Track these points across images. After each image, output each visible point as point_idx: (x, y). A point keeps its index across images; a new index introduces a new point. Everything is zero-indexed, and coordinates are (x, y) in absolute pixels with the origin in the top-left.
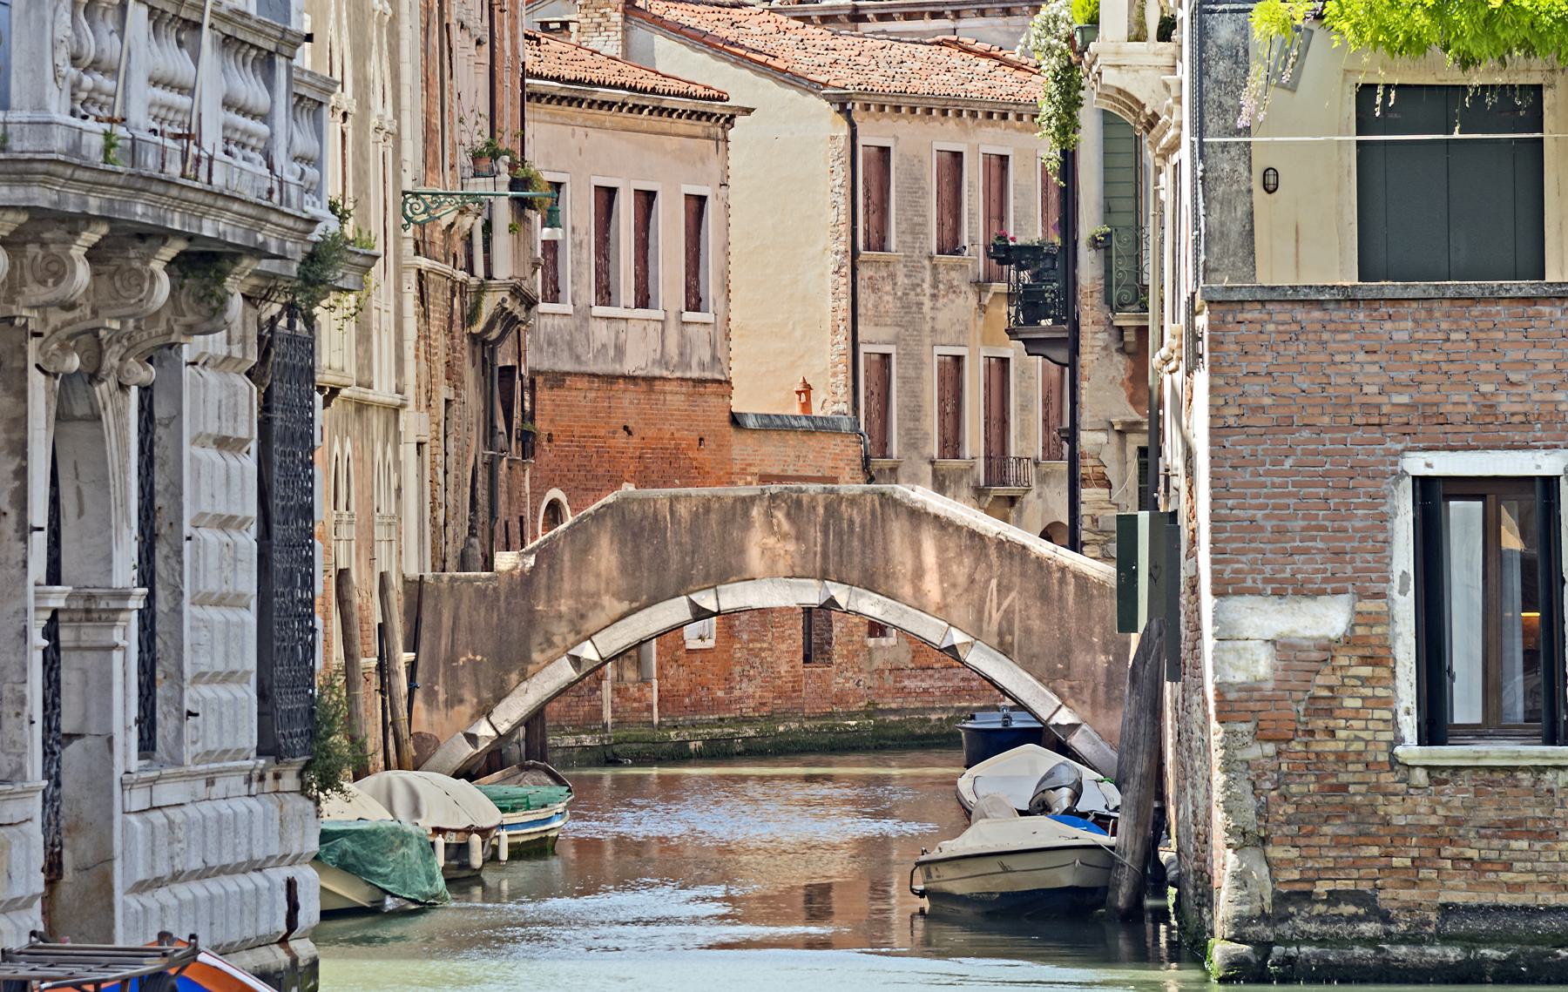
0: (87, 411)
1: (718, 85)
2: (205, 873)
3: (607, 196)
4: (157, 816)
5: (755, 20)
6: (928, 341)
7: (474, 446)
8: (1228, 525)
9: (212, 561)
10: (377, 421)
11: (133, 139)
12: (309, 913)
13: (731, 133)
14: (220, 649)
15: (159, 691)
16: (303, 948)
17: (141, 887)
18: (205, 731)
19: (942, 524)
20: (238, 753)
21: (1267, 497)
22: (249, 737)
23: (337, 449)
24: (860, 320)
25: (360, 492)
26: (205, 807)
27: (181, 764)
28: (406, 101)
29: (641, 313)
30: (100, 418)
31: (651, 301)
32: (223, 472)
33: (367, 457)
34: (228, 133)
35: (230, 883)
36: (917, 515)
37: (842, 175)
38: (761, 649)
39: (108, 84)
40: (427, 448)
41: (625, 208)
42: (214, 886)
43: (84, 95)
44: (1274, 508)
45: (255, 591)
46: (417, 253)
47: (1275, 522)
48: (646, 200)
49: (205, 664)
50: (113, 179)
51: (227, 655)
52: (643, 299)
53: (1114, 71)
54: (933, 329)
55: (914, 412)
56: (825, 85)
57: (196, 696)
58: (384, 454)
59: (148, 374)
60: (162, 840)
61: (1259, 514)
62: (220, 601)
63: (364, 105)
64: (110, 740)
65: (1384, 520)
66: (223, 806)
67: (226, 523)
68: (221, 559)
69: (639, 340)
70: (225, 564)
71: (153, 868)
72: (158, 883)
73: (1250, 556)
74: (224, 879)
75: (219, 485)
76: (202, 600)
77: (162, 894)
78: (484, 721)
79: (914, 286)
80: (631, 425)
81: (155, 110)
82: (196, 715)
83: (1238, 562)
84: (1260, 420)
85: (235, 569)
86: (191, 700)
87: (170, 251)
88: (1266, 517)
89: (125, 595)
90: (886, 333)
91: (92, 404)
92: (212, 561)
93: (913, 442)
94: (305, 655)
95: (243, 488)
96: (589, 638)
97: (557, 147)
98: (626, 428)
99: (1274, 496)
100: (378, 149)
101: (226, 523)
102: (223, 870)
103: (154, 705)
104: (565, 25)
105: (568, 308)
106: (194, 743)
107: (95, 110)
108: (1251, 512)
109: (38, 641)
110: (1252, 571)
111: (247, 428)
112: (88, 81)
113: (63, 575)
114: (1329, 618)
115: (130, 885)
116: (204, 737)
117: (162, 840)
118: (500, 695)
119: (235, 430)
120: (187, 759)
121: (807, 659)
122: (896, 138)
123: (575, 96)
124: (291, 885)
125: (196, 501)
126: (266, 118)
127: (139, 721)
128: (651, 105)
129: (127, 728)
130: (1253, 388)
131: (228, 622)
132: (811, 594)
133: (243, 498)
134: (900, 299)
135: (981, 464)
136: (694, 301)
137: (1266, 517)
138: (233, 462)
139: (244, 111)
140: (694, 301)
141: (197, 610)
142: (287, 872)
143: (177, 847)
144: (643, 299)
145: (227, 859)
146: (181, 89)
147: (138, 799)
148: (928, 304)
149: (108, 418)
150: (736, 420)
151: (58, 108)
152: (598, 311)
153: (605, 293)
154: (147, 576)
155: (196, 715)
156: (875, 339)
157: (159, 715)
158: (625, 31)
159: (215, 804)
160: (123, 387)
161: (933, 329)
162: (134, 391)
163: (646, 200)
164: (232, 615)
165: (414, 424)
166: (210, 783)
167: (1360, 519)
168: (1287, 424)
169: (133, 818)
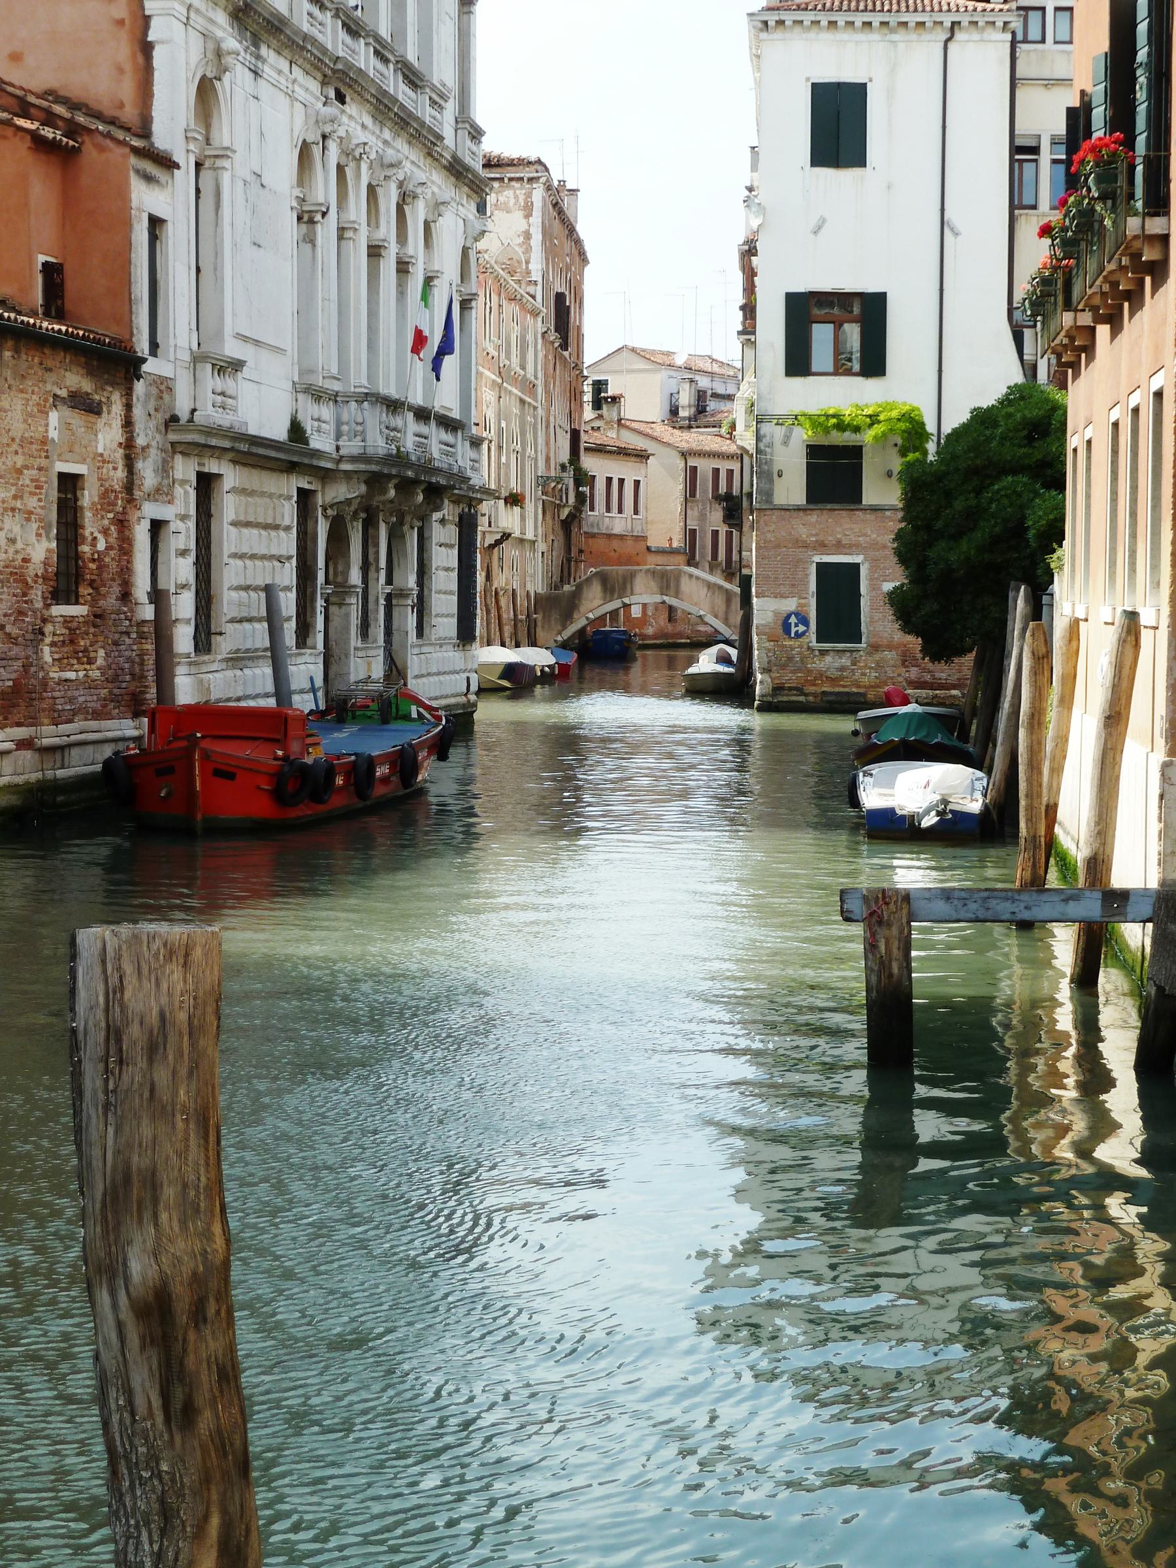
2: (439, 674)
3: (609, 480)
10: (527, 546)
12: (474, 687)
16: (472, 698)
17: (416, 677)
22: (453, 632)
35: (447, 677)
42: (441, 678)
48: (621, 481)
52: (620, 511)
55: (703, 547)
63: (524, 449)
65: (807, 575)
67: (447, 569)
69: (618, 524)
72: (422, 676)
75: (445, 558)
76: (439, 592)
87: (395, 481)
93: (703, 556)
97: (589, 463)
100: (528, 464)
101: (447, 569)
109: (382, 601)
114: (790, 605)
118: (564, 627)
123: (599, 450)
128: (623, 453)
130: (769, 536)
136: (636, 512)
140: (636, 512)
144: (620, 511)
147: (416, 651)
150: (648, 549)
151: (381, 442)
153: (608, 510)
156: (692, 525)
163: (621, 481)
165: (542, 546)
167: (800, 575)
168: (778, 546)
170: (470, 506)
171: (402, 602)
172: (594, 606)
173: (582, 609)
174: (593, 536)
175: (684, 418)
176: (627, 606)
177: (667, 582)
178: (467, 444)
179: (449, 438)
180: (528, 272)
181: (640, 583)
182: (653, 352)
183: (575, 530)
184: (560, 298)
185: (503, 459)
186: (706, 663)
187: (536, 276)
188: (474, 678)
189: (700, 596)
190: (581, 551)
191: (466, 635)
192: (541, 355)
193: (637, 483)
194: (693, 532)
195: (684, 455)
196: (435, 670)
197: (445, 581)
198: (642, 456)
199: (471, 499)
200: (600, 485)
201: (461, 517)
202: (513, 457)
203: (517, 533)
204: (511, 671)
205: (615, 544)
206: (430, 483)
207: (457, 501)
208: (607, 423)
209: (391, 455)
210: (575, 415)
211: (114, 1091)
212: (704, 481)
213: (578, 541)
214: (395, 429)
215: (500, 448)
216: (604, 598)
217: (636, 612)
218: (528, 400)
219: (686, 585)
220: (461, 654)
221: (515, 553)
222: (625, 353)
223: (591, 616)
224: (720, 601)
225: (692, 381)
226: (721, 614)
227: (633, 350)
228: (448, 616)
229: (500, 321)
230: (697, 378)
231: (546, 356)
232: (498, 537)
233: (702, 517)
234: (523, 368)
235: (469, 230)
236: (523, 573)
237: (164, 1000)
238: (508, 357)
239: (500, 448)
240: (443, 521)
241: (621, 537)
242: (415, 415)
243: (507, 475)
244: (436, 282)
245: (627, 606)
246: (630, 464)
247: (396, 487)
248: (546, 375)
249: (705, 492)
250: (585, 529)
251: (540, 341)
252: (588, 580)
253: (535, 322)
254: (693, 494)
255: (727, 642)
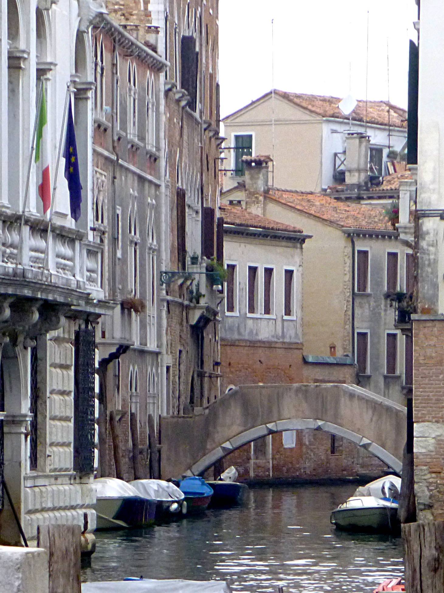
0: (13, 355)
1: (298, 227)
2: (54, 509)
3: (253, 270)
4: (37, 489)
5: (317, 199)
6: (382, 327)
7: (193, 366)
8: (420, 398)
9: (57, 405)
11: (24, 269)
12: (92, 525)
13: (304, 246)
14: (60, 434)
15: (38, 448)
17: (30, 512)
18: (54, 462)
19: (361, 398)
20: (67, 470)
21: (434, 388)
23: (131, 368)
24: (355, 320)
25: (141, 385)
26: (55, 488)
27: (45, 472)
28: (163, 237)
29: (267, 316)
30: (17, 357)
31: (271, 311)
32: (61, 375)
33: (144, 371)
34: (58, 265)
36: (352, 396)
37: (349, 262)
38: (314, 448)
39: (15, 251)
40: (171, 369)
41: (261, 275)
42: (57, 514)
43: (7, 255)
44: (437, 392)
45: (73, 415)
46: (167, 294)
47: (436, 397)
48: (269, 272)
49: (54, 439)
50: (16, 282)
51: (62, 436)
52: (267, 310)
53: (404, 234)
54: (385, 324)
55: (376, 356)
56: (343, 226)
57: (51, 450)
58: (152, 370)
59: (34, 343)
60: (38, 496)
61: (431, 394)
62: (61, 419)
64: (20, 463)
66: (61, 488)
67: (63, 393)
68: (60, 404)
69: (265, 327)
70: (62, 407)
71: (35, 506)
72: (36, 511)
73: (428, 409)
74: (61, 512)
75: (60, 380)
76: (53, 418)
77: (39, 515)
78: (189, 471)
79: (377, 306)
80: (262, 360)
81: (32, 259)
82: (51, 456)
83: (423, 411)
84: (433, 361)
85: (65, 409)
86: (49, 451)
87: (11, 300)
88: (434, 396)
89: (26, 416)
90: (366, 324)
91: (15, 353)
92: (57, 405)
93: (375, 368)
94: (91, 438)
95: (69, 380)
96: (228, 440)
98: (260, 361)
99: (436, 388)
101: (63, 393)
102: (60, 509)
103: (36, 453)
104: (239, 202)
105: (238, 314)
106: (50, 465)
107: (11, 260)
108: (427, 394)
110: (428, 414)
111: (72, 361)
112: (8, 251)
113: (5, 408)
115: (26, 511)
116: (54, 464)
117: (38, 496)
119: (66, 362)
120: (48, 470)
121: (333, 452)
122: (371, 247)
123: (242, 232)
124: (86, 516)
125: (51, 385)
126: (71, 259)
127: (30, 457)
129: (26, 460)
131: (62, 426)
132: (313, 424)
133: (69, 384)
134: (372, 311)
135: (404, 376)
136: (288, 312)
137: (434, 396)
138: (65, 372)
139: (64, 258)
140: (288, 312)
141: (52, 422)
142: (84, 511)
143: (43, 499)
144: (267, 310)
145: (62, 504)
146: (42, 252)
147: (29, 483)
148: (383, 314)
149: (20, 359)
152: (249, 315)
153: (252, 309)
154: (34, 409)
155: (51, 456)
157: (38, 456)
158: (264, 204)
159: (58, 486)
160: (26, 348)
161: (385, 324)
162: (29, 349)
164: (64, 424)
165: (167, 360)
166: (56, 479)
169: (28, 489)
170: (87, 322)
171: (15, 429)
172: (232, 431)
173: (218, 437)
174: (233, 344)
175: (352, 187)
176: (276, 434)
177: (323, 404)
178: (85, 252)
179: (66, 250)
180: (148, 14)
181: (289, 404)
182: (312, 99)
183: (208, 335)
184: (187, 44)
185: (119, 254)
186: (366, 500)
187: (158, 21)
188: (92, 513)
189: (359, 420)
190: (217, 364)
191: (83, 467)
192: (163, 119)
193: (289, 274)
194: (363, 336)
195: (352, 236)
196: (50, 505)
197: (60, 405)
198: (296, 239)
199: (89, 314)
200: (241, 278)
201: (77, 334)
202: (131, 250)
203: (137, 344)
204: (130, 508)
205: (261, 353)
206: (46, 301)
207: (73, 316)
208: (251, 194)
209: (7, 274)
210: (209, 191)
211: (52, 571)
212: (377, 270)
213: (213, 350)
214: (12, 246)
215: (115, 240)
216: (245, 423)
217: (289, 441)
218: (149, 177)
219: (346, 409)
220: (78, 487)
221: (133, 369)
222: (274, 101)
223: (227, 445)
224: (388, 426)
225: (361, 137)
226: (389, 443)
227: (285, 96)
228: (63, 445)
229: (114, 82)
230: (370, 132)
231: (170, 120)
232: (114, 350)
233: (375, 318)
234: (142, 138)
235: (84, 11)
236: (150, 395)
237: (67, 544)
238: (124, 127)
239: (115, 240)
240: (56, 340)
241: (269, 345)
242: (31, 227)
243: (124, 274)
244: (49, 75)
245: (276, 434)
246: (280, 250)
247: (11, 306)
248: (170, 144)
249: (377, 284)
250: (220, 334)
251: (163, 102)
252: (225, 402)
253: (157, 78)
254: (363, 286)
255: (395, 474)
